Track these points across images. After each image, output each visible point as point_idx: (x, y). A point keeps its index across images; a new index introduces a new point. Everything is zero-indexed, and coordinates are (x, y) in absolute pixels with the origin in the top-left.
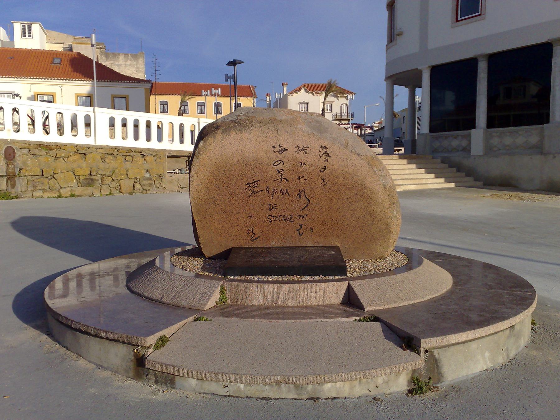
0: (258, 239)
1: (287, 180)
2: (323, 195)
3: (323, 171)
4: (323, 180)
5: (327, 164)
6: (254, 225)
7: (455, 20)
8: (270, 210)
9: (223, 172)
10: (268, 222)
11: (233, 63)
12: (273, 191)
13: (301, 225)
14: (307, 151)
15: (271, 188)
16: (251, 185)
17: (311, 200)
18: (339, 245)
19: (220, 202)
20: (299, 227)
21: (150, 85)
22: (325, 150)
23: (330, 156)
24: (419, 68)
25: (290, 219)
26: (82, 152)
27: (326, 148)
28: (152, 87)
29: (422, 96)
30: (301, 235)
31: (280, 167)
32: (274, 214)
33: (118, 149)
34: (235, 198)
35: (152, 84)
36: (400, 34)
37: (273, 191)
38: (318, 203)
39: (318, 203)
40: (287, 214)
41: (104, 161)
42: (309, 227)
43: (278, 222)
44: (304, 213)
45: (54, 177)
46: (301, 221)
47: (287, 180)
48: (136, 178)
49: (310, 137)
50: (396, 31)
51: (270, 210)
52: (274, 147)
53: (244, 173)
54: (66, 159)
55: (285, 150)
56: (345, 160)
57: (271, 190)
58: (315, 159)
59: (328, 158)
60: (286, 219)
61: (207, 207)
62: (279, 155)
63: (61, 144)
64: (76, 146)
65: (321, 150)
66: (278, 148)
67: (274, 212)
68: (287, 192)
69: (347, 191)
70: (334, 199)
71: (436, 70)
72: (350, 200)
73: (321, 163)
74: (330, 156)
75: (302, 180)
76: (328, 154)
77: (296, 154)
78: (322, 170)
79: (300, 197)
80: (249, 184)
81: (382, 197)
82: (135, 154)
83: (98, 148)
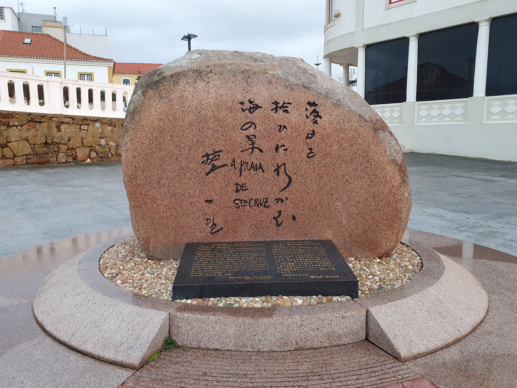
0: (221, 232)
1: (261, 151)
2: (309, 171)
3: (310, 138)
4: (311, 149)
5: (315, 127)
6: (216, 212)
7: (388, 2)
8: (237, 191)
9: (169, 138)
10: (235, 208)
11: (188, 38)
12: (242, 165)
13: (280, 212)
14: (289, 109)
15: (239, 162)
16: (211, 157)
17: (294, 178)
18: (330, 237)
19: (167, 181)
20: (277, 214)
21: (113, 64)
22: (314, 108)
23: (320, 117)
24: (355, 46)
25: (264, 204)
26: (34, 120)
27: (316, 105)
28: (114, 65)
29: (359, 72)
30: (280, 225)
31: (251, 131)
32: (243, 198)
33: (73, 118)
34: (188, 175)
35: (115, 63)
36: (338, 16)
37: (242, 165)
38: (303, 181)
39: (303, 181)
40: (261, 196)
41: (59, 130)
42: (290, 214)
43: (247, 208)
44: (284, 195)
45: (7, 146)
46: (280, 206)
47: (261, 151)
48: (92, 146)
49: (292, 90)
50: (334, 13)
51: (237, 191)
52: (242, 103)
53: (200, 140)
54: (19, 128)
55: (257, 107)
56: (342, 121)
57: (238, 166)
58: (300, 121)
59: (318, 119)
60: (258, 203)
61: (148, 188)
62: (250, 115)
63: (14, 112)
64: (30, 114)
65: (308, 107)
66: (248, 105)
67: (242, 195)
68: (261, 167)
69: (344, 166)
70: (325, 176)
71: (368, 47)
72: (347, 177)
73: (310, 126)
74: (320, 117)
75: (281, 150)
76: (318, 112)
77: (273, 113)
78: (310, 136)
79: (278, 174)
80: (207, 155)
81: (390, 173)
82: (90, 122)
83: (51, 117)
